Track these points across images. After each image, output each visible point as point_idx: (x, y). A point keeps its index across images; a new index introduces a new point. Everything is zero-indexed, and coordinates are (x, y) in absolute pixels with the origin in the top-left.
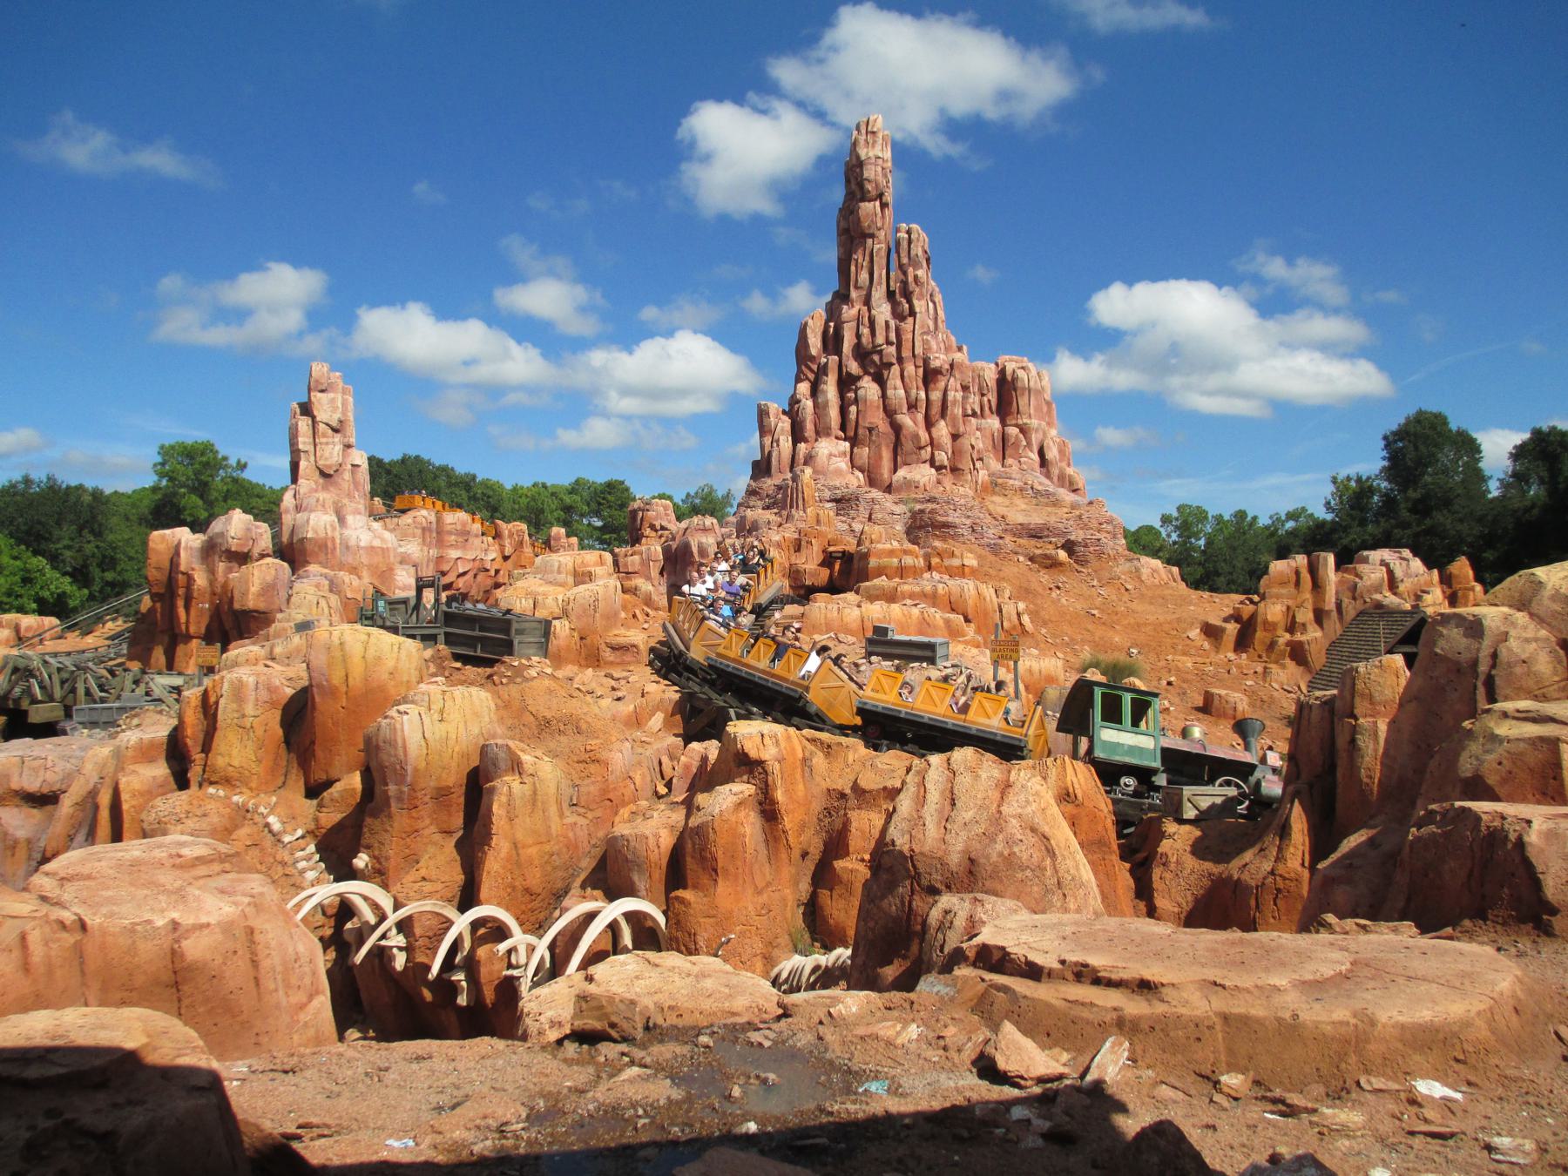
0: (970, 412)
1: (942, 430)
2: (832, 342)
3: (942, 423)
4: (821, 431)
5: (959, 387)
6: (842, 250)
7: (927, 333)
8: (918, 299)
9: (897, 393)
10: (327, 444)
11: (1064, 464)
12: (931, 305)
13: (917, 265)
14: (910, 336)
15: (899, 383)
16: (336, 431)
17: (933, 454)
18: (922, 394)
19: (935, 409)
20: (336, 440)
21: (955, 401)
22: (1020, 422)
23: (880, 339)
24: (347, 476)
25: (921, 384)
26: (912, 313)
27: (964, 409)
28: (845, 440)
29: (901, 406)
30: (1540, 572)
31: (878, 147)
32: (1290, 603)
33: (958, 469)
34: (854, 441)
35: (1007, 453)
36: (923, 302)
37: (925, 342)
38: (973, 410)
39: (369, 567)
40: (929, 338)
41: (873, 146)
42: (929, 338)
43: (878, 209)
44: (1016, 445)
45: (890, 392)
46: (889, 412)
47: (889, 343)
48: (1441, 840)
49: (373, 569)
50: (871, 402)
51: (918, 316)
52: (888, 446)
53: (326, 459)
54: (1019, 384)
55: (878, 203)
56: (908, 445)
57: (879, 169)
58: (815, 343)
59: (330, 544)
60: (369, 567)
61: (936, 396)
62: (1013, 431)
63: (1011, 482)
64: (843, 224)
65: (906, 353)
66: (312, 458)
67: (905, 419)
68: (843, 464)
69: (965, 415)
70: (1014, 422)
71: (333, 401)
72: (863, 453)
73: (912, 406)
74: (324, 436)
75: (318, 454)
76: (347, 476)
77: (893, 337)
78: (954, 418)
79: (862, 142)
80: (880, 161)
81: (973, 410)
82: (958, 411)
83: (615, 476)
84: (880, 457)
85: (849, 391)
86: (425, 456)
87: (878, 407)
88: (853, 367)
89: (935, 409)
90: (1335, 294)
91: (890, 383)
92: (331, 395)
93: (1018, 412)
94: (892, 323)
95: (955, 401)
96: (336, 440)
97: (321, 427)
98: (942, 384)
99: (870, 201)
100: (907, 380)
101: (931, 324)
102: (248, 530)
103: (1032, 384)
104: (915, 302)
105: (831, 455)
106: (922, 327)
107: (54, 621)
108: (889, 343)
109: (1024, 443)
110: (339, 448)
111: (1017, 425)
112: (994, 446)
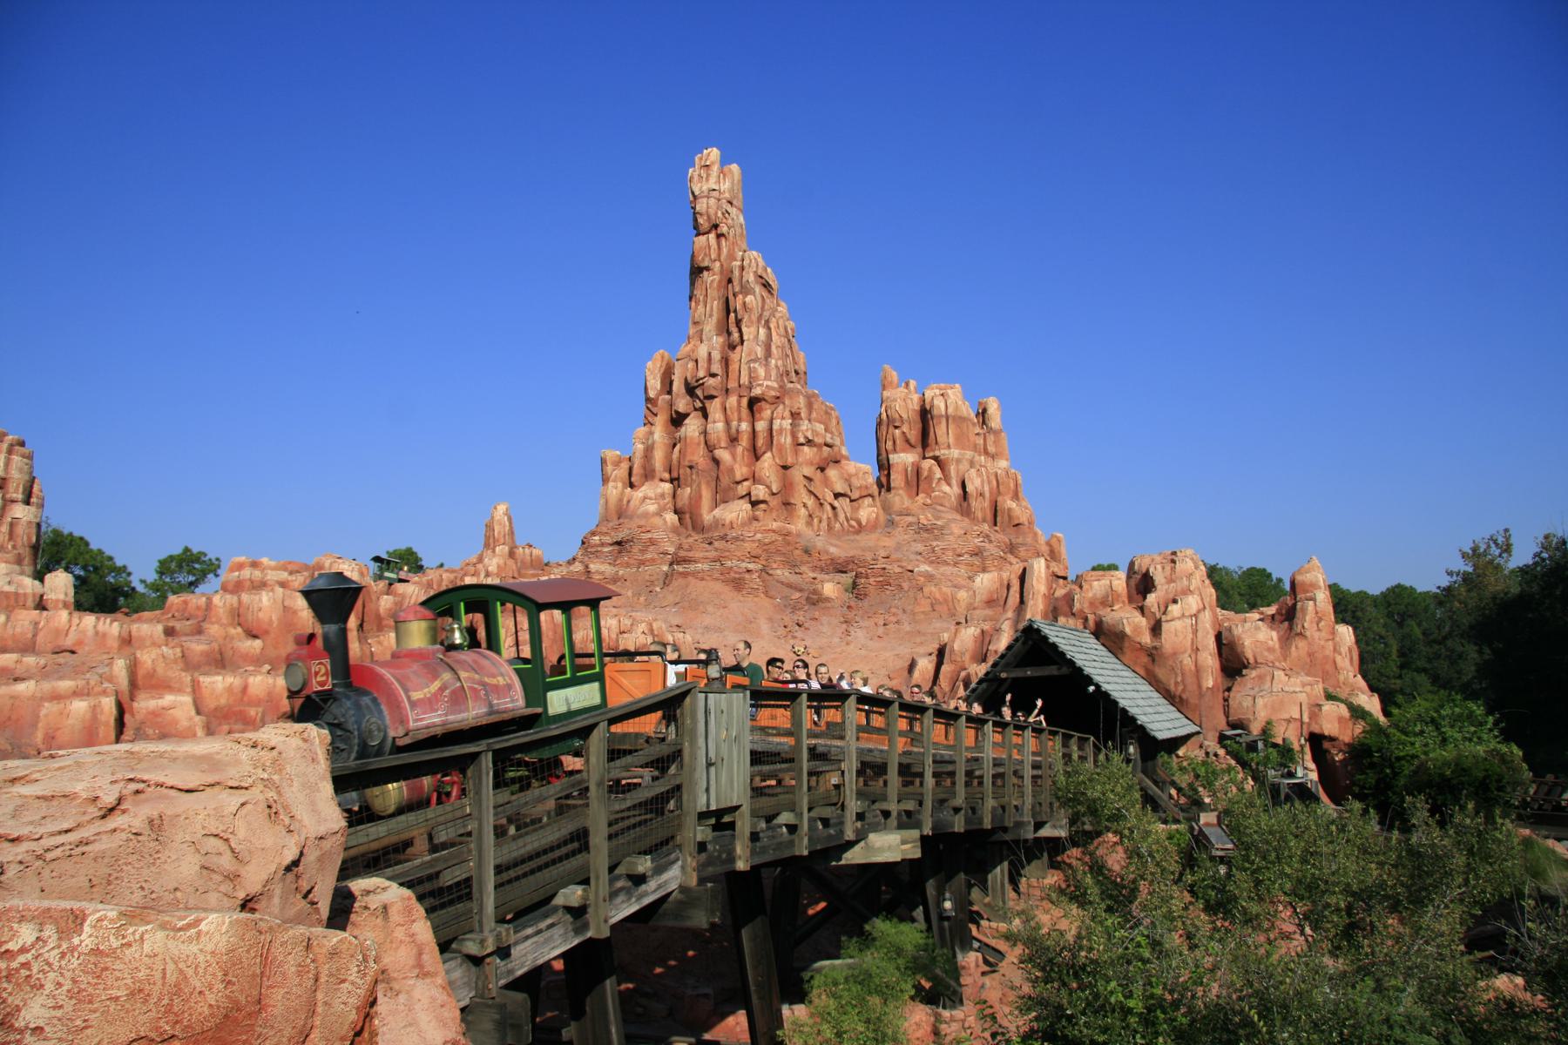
1: (767, 463)
2: (668, 386)
3: (768, 455)
4: (648, 475)
5: (787, 414)
7: (756, 360)
8: (747, 326)
12: (762, 331)
13: (746, 290)
18: (745, 426)
19: (760, 442)
21: (781, 431)
22: (937, 453)
27: (794, 436)
29: (719, 441)
31: (713, 180)
32: (986, 627)
33: (789, 504)
35: (920, 488)
36: (753, 329)
38: (806, 437)
40: (756, 365)
41: (707, 180)
44: (930, 478)
46: (710, 448)
50: (692, 438)
52: (708, 483)
54: (935, 412)
55: (712, 236)
58: (655, 384)
61: (761, 426)
67: (724, 455)
70: (931, 454)
73: (733, 440)
78: (781, 449)
79: (696, 178)
80: (715, 194)
81: (806, 437)
82: (786, 440)
83: (409, 545)
86: (397, 548)
88: (682, 404)
93: (937, 443)
95: (781, 431)
98: (767, 413)
99: (704, 234)
101: (760, 351)
103: (950, 411)
104: (744, 329)
106: (749, 354)
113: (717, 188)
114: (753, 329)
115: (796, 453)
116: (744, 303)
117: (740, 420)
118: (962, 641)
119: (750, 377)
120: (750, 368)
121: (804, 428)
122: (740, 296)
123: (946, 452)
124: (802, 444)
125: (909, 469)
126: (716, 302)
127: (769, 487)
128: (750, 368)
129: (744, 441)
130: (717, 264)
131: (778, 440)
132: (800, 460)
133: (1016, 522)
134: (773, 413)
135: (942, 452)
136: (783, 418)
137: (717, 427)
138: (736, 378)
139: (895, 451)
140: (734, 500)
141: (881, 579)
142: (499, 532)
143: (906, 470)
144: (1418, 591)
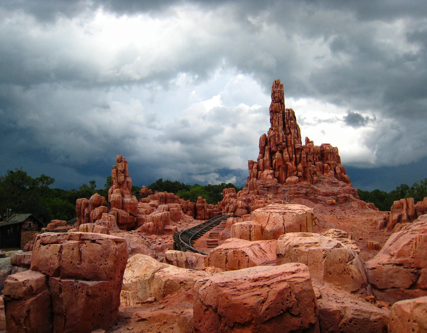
0: (308, 160)
1: (300, 166)
5: (305, 153)
6: (271, 117)
8: (292, 129)
9: (286, 156)
10: (120, 176)
11: (343, 174)
12: (296, 130)
14: (290, 139)
15: (287, 153)
16: (122, 172)
17: (297, 173)
18: (294, 156)
19: (298, 160)
20: (123, 175)
21: (304, 158)
22: (328, 162)
23: (281, 141)
24: (125, 184)
25: (293, 153)
26: (290, 133)
27: (307, 160)
28: (272, 170)
30: (77, 211)
34: (274, 170)
36: (293, 130)
37: (294, 141)
38: (309, 159)
39: (130, 208)
40: (296, 140)
41: (278, 88)
42: (296, 140)
43: (280, 105)
44: (327, 169)
45: (284, 156)
47: (283, 142)
48: (22, 186)
49: (131, 209)
51: (292, 134)
53: (120, 180)
56: (290, 171)
57: (280, 94)
59: (119, 202)
60: (130, 208)
61: (298, 156)
62: (326, 165)
63: (325, 180)
64: (271, 109)
65: (289, 144)
66: (116, 180)
68: (270, 177)
69: (307, 161)
71: (122, 165)
72: (277, 173)
74: (120, 174)
75: (118, 179)
76: (125, 184)
77: (285, 140)
81: (309, 159)
84: (282, 174)
85: (273, 156)
87: (281, 160)
89: (298, 160)
90: (70, 227)
91: (284, 153)
92: (122, 163)
94: (284, 136)
96: (123, 175)
97: (119, 171)
100: (289, 152)
101: (296, 136)
102: (99, 199)
103: (331, 151)
105: (267, 174)
107: (65, 221)
108: (283, 142)
109: (330, 168)
110: (123, 177)
111: (327, 163)
112: (320, 170)
113: (280, 90)
114: (293, 130)
115: (307, 164)
116: (291, 123)
117: (293, 154)
118: (395, 217)
119: (294, 143)
120: (294, 140)
121: (309, 157)
122: (289, 121)
123: (330, 162)
124: (309, 161)
125: (321, 166)
126: (282, 122)
127: (302, 172)
128: (294, 140)
129: (294, 160)
130: (281, 111)
131: (303, 160)
132: (308, 165)
133: (346, 181)
134: (301, 153)
135: (330, 162)
136: (304, 154)
137: (286, 156)
138: (290, 143)
139: (316, 161)
140: (293, 176)
141: (345, 199)
142: (255, 186)
143: (320, 166)
144: (369, 192)
